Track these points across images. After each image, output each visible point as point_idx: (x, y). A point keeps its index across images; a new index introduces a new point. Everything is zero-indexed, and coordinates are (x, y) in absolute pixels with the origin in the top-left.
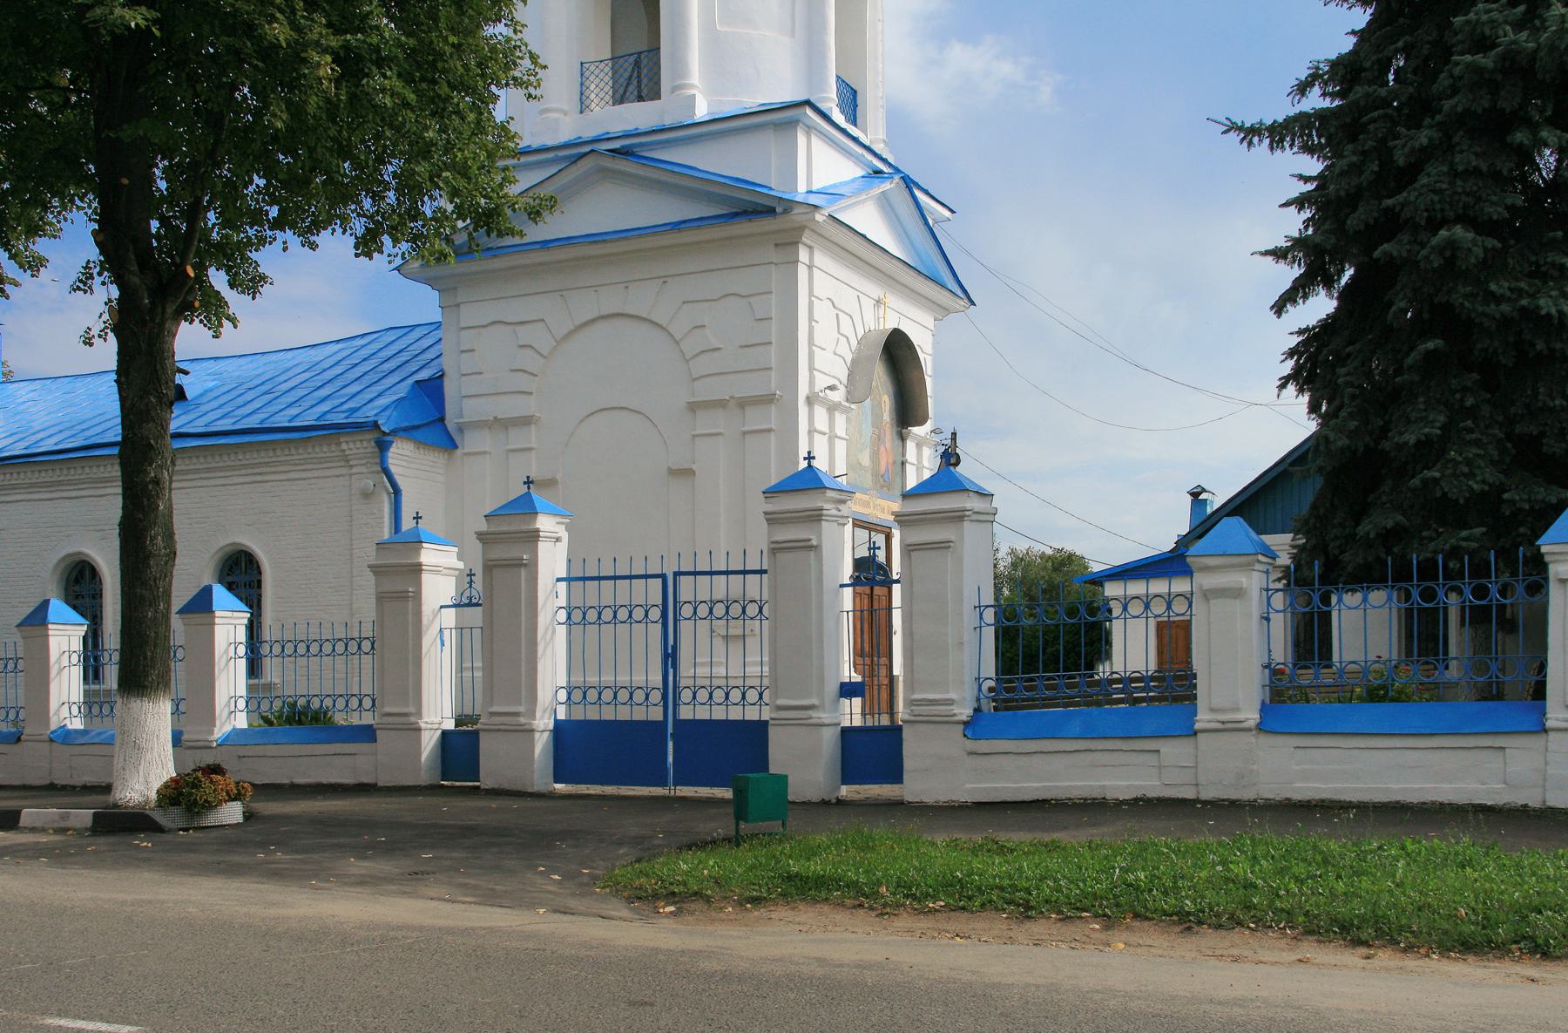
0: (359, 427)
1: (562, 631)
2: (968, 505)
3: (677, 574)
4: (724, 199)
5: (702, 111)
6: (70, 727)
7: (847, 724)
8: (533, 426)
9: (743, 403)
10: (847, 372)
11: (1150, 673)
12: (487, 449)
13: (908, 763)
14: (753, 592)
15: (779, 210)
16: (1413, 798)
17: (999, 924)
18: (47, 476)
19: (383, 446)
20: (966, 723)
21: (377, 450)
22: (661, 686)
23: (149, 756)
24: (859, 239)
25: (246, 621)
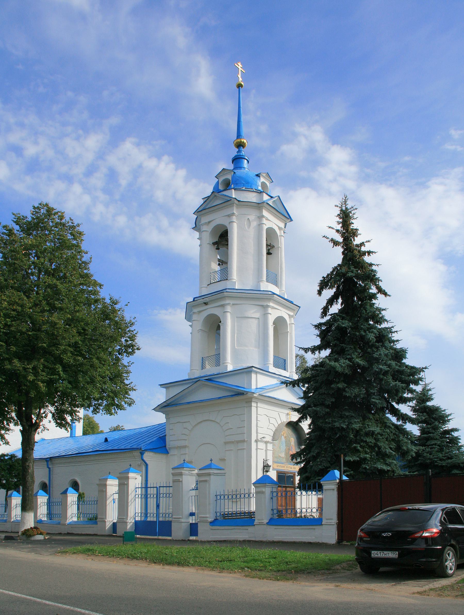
0: (137, 449)
2: (211, 472)
3: (160, 487)
4: (233, 391)
5: (230, 368)
6: (43, 520)
7: (191, 522)
8: (187, 448)
9: (238, 442)
14: (171, 491)
16: (298, 541)
17: (126, 561)
18: (69, 461)
19: (142, 454)
20: (211, 523)
23: (27, 525)
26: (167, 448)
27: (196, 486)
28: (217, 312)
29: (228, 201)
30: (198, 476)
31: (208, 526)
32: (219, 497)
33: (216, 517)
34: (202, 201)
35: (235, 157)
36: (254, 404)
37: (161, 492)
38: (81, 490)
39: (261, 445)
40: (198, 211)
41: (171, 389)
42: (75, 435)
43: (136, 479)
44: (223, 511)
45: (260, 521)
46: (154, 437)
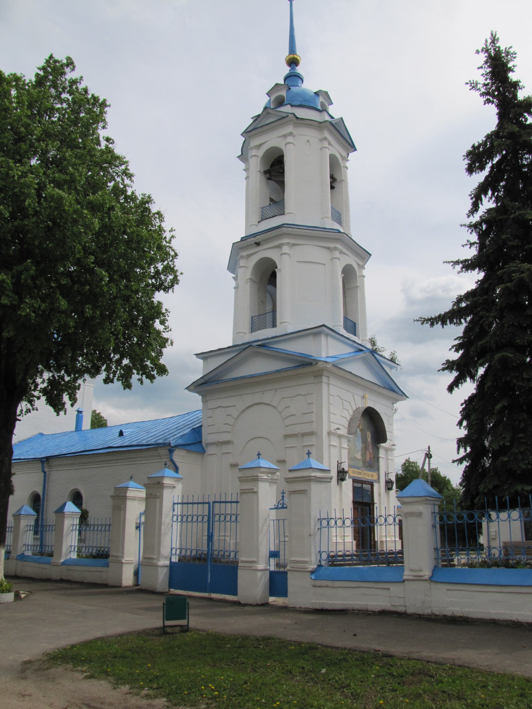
1: (177, 526)
3: (214, 502)
9: (304, 435)
10: (348, 423)
11: (388, 551)
12: (230, 451)
13: (290, 589)
15: (314, 363)
16: (501, 617)
19: (171, 451)
20: (312, 572)
21: (169, 453)
22: (207, 550)
24: (349, 374)
25: (79, 516)
26: (204, 445)
27: (281, 502)
28: (273, 254)
29: (284, 117)
30: (287, 482)
31: (307, 581)
32: (324, 523)
33: (320, 561)
34: (252, 121)
35: (289, 75)
36: (324, 379)
37: (217, 511)
38: (84, 506)
39: (335, 442)
40: (246, 131)
41: (210, 360)
42: (81, 429)
43: (174, 487)
44: (334, 550)
45: (416, 574)
46: (186, 428)
